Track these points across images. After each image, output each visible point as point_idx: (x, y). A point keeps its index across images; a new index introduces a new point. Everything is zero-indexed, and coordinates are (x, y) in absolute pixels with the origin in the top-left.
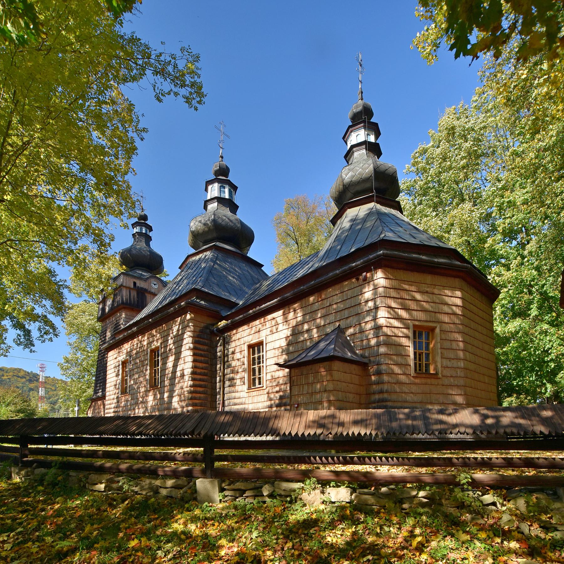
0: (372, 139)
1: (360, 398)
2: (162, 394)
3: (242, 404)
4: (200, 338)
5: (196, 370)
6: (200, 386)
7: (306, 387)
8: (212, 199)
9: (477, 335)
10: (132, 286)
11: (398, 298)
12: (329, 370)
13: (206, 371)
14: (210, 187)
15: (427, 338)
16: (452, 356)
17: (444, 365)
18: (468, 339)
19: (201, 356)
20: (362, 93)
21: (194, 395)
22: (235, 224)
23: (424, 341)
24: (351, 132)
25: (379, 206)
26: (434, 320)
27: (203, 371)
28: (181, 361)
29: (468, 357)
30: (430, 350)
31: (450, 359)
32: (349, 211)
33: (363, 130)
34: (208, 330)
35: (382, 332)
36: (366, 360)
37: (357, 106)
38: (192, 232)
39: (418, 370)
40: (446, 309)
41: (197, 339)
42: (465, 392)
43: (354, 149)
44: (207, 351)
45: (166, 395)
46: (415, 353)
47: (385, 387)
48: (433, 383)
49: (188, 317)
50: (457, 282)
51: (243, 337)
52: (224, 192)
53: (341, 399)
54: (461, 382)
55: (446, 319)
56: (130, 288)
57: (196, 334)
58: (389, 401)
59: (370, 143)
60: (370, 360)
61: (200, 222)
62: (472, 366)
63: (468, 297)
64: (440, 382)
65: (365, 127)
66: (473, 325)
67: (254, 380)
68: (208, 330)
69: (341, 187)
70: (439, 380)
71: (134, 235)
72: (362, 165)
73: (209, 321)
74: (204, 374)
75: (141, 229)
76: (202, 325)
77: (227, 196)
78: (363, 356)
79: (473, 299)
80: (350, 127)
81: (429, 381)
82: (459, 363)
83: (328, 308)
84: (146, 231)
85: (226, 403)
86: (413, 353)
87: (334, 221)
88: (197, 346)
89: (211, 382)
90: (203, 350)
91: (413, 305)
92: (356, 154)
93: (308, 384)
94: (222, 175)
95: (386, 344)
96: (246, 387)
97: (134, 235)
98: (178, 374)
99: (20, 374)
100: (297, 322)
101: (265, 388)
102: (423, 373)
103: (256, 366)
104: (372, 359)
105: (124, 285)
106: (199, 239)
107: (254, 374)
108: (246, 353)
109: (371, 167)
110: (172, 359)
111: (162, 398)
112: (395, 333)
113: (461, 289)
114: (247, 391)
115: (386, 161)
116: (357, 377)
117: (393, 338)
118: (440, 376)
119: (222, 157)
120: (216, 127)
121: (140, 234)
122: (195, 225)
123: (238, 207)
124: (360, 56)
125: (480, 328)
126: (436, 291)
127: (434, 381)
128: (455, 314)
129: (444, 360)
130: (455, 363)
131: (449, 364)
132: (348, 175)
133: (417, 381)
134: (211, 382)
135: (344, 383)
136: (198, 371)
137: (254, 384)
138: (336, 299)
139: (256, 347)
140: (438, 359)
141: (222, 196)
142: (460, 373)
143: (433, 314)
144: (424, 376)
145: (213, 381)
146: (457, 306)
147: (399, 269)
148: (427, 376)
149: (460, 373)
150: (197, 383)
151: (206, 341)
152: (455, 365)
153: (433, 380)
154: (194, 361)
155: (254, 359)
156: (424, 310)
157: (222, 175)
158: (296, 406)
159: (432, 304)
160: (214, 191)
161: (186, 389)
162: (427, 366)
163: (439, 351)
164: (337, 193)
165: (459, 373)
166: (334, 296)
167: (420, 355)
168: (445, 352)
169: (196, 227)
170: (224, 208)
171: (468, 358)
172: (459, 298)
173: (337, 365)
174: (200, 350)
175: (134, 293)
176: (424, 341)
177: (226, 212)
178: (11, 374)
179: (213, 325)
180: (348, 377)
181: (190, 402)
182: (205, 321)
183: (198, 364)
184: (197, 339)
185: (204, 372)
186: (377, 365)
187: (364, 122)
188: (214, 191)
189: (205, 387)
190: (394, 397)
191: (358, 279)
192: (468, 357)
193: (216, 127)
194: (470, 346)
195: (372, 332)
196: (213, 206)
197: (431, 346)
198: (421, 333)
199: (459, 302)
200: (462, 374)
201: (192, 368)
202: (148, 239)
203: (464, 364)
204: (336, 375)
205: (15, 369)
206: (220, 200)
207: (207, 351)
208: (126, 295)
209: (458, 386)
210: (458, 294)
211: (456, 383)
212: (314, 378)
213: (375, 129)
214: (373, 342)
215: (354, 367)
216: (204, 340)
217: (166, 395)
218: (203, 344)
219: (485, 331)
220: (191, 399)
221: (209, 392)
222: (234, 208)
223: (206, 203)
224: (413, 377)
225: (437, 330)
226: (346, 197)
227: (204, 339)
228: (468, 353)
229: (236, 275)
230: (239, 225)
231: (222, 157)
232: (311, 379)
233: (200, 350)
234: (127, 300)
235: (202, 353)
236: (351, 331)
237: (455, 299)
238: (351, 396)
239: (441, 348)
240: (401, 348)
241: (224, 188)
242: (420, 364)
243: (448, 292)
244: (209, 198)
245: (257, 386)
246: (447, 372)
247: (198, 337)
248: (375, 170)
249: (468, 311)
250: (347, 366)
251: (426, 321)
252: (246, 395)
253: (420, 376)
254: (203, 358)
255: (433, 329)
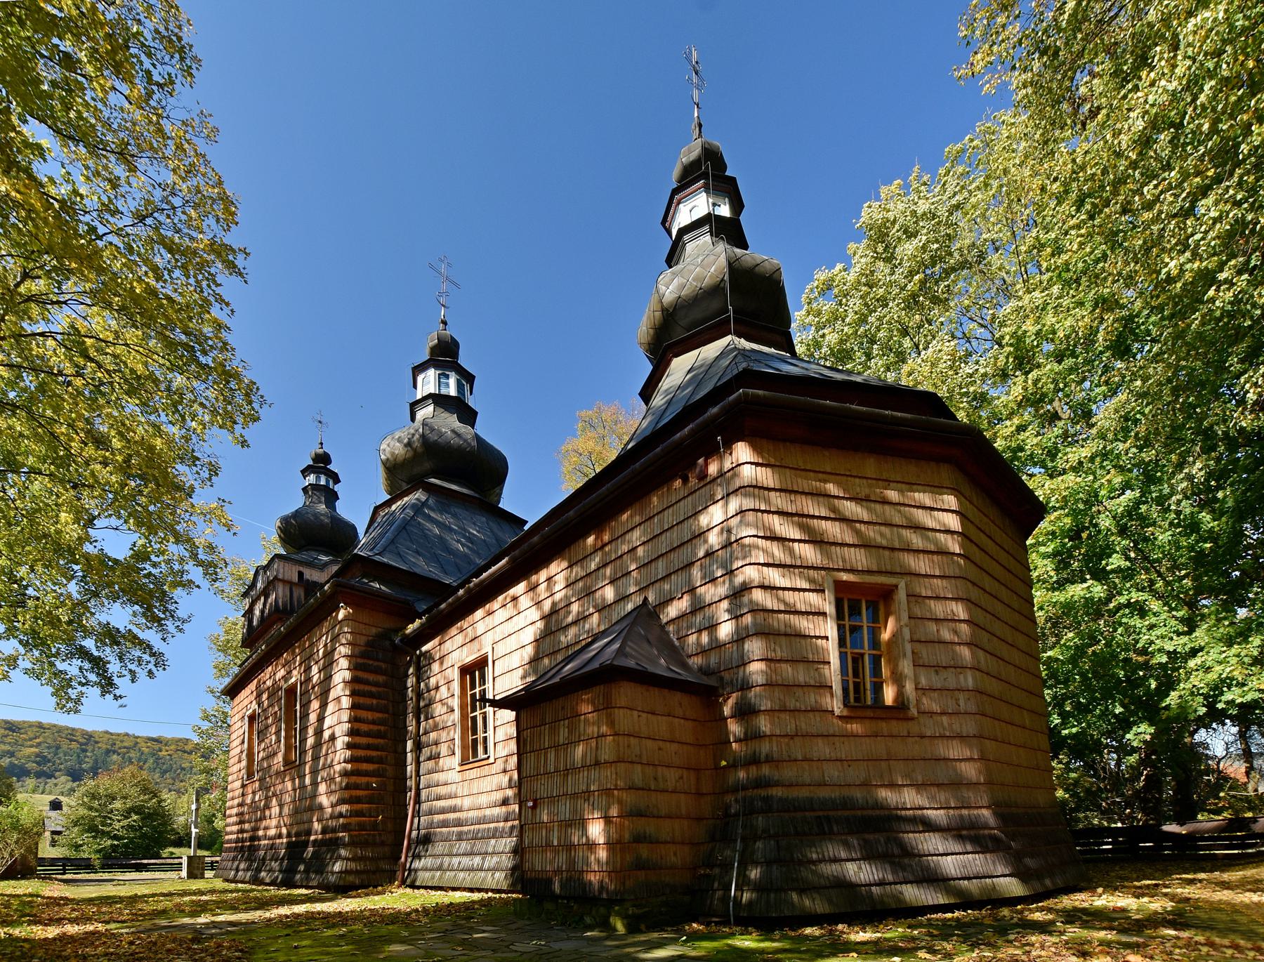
0: (724, 211)
1: (698, 779)
2: (302, 777)
3: (450, 797)
4: (369, 658)
5: (357, 725)
6: (368, 760)
7: (552, 755)
8: (425, 398)
9: (999, 608)
10: (295, 579)
11: (792, 515)
12: (606, 707)
13: (382, 728)
14: (420, 378)
15: (875, 619)
16: (944, 659)
17: (923, 682)
18: (981, 617)
19: (371, 695)
20: (700, 126)
21: (354, 779)
22: (465, 441)
23: (865, 624)
24: (679, 203)
25: (744, 344)
26: (889, 568)
27: (375, 728)
28: (331, 708)
29: (982, 660)
30: (883, 648)
31: (938, 668)
32: (676, 362)
33: (704, 194)
34: (387, 643)
35: (751, 601)
36: (712, 682)
37: (691, 152)
38: (384, 463)
39: (852, 700)
40: (916, 540)
41: (360, 661)
42: (981, 751)
43: (686, 237)
44: (385, 685)
45: (308, 781)
46: (843, 657)
47: (765, 748)
48: (895, 732)
49: (341, 614)
50: (946, 474)
51: (453, 650)
52: (447, 385)
53: (640, 784)
54: (969, 727)
55: (921, 565)
56: (291, 583)
57: (357, 650)
58: (777, 784)
59: (718, 218)
60: (722, 679)
61: (399, 440)
62: (993, 686)
63: (972, 512)
64: (914, 728)
65: (706, 188)
66: (988, 583)
67: (475, 742)
68: (387, 643)
69: (658, 314)
70: (910, 723)
71: (305, 490)
72: (706, 260)
73: (388, 623)
74: (378, 735)
75: (318, 478)
76: (374, 631)
77: (452, 391)
78: (705, 671)
79: (985, 519)
80: (675, 192)
81: (884, 726)
82: (961, 677)
83: (618, 562)
84: (327, 482)
85: (424, 794)
86: (837, 654)
87: (647, 393)
88: (360, 674)
89: (396, 752)
90: (376, 684)
91: (833, 530)
92: (689, 247)
93: (556, 747)
94: (445, 355)
95: (764, 633)
96: (457, 758)
97: (305, 490)
98: (326, 735)
99: (188, 748)
100: (554, 604)
101: (491, 760)
102: (868, 707)
103: (477, 713)
104: (726, 676)
105: (280, 576)
106: (401, 475)
107: (475, 732)
108: (456, 686)
109: (722, 261)
110: (315, 705)
111: (302, 787)
112: (786, 604)
113: (955, 491)
114: (458, 768)
115: (758, 253)
116: (689, 724)
117: (781, 616)
118: (914, 711)
119: (445, 323)
120: (431, 266)
121: (315, 487)
122: (392, 446)
123: (475, 413)
124: (695, 54)
125: (1004, 594)
126: (893, 495)
127: (896, 727)
128: (943, 552)
129: (922, 671)
130: (950, 679)
131: (937, 681)
132: (672, 286)
133: (855, 727)
134: (396, 752)
135: (649, 743)
136: (364, 727)
137: (475, 754)
138: (636, 537)
139: (474, 670)
140: (906, 667)
141: (444, 391)
142: (964, 703)
143: (887, 553)
144: (869, 713)
145: (400, 749)
146: (948, 531)
147: (793, 441)
148: (879, 713)
149: (964, 703)
150: (361, 753)
151: (383, 666)
152: (952, 683)
153: (894, 723)
154: (354, 707)
155: (473, 696)
156: (866, 545)
157: (445, 355)
158: (530, 804)
159: (883, 528)
160: (428, 382)
161: (338, 768)
162: (878, 688)
163: (908, 647)
164: (651, 331)
165: (962, 703)
166: (633, 536)
167: (855, 660)
168: (924, 651)
169: (393, 454)
170: (446, 415)
171: (983, 666)
172: (953, 511)
173: (625, 693)
174: (367, 682)
175: (299, 593)
176: (865, 624)
177: (449, 423)
178: (173, 747)
179: (397, 631)
180: (661, 725)
181: (346, 794)
182: (377, 624)
183: (363, 714)
184: (360, 661)
185: (379, 731)
186: (742, 689)
187: (705, 176)
188: (428, 382)
189: (380, 761)
190: (789, 773)
191: (685, 480)
192: (982, 660)
193: (431, 266)
194: (985, 636)
195: (725, 605)
196: (426, 412)
197: (886, 636)
198: (859, 602)
199: (953, 522)
200: (972, 708)
201: (349, 722)
202: (332, 497)
203: (974, 678)
204: (625, 719)
205: (180, 740)
206: (439, 400)
207: (385, 685)
208: (284, 596)
209: (960, 737)
210: (951, 501)
211: (956, 727)
212: (570, 732)
213: (726, 187)
214: (725, 630)
215: (677, 700)
216: (376, 664)
217: (308, 781)
218: (376, 671)
219: (1016, 603)
220: (347, 787)
221: (390, 771)
222: (468, 416)
223: (414, 406)
224: (840, 717)
225: (901, 595)
226: (672, 334)
227: (378, 660)
228: (981, 654)
229: (464, 537)
230: (474, 443)
231: (445, 323)
232: (563, 734)
233: (367, 682)
234: (285, 604)
235: (373, 689)
236: (673, 611)
237: (942, 514)
238: (671, 776)
239: (912, 641)
240: (803, 641)
241: (447, 377)
242: (856, 685)
243: (925, 498)
244: (419, 397)
245: (481, 755)
246: (930, 704)
247: (363, 655)
248: (730, 264)
249: (975, 548)
250: (655, 697)
251: (869, 572)
252: (458, 777)
253: (859, 713)
254: (375, 702)
255: (887, 594)
